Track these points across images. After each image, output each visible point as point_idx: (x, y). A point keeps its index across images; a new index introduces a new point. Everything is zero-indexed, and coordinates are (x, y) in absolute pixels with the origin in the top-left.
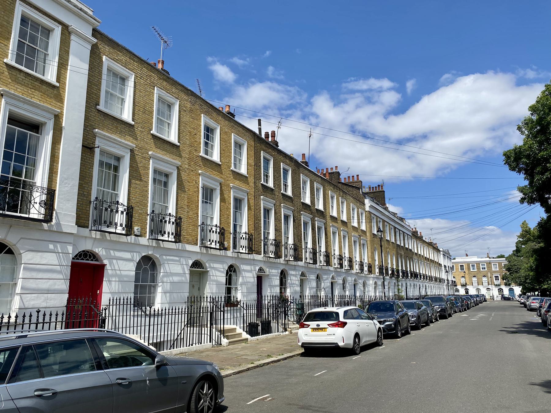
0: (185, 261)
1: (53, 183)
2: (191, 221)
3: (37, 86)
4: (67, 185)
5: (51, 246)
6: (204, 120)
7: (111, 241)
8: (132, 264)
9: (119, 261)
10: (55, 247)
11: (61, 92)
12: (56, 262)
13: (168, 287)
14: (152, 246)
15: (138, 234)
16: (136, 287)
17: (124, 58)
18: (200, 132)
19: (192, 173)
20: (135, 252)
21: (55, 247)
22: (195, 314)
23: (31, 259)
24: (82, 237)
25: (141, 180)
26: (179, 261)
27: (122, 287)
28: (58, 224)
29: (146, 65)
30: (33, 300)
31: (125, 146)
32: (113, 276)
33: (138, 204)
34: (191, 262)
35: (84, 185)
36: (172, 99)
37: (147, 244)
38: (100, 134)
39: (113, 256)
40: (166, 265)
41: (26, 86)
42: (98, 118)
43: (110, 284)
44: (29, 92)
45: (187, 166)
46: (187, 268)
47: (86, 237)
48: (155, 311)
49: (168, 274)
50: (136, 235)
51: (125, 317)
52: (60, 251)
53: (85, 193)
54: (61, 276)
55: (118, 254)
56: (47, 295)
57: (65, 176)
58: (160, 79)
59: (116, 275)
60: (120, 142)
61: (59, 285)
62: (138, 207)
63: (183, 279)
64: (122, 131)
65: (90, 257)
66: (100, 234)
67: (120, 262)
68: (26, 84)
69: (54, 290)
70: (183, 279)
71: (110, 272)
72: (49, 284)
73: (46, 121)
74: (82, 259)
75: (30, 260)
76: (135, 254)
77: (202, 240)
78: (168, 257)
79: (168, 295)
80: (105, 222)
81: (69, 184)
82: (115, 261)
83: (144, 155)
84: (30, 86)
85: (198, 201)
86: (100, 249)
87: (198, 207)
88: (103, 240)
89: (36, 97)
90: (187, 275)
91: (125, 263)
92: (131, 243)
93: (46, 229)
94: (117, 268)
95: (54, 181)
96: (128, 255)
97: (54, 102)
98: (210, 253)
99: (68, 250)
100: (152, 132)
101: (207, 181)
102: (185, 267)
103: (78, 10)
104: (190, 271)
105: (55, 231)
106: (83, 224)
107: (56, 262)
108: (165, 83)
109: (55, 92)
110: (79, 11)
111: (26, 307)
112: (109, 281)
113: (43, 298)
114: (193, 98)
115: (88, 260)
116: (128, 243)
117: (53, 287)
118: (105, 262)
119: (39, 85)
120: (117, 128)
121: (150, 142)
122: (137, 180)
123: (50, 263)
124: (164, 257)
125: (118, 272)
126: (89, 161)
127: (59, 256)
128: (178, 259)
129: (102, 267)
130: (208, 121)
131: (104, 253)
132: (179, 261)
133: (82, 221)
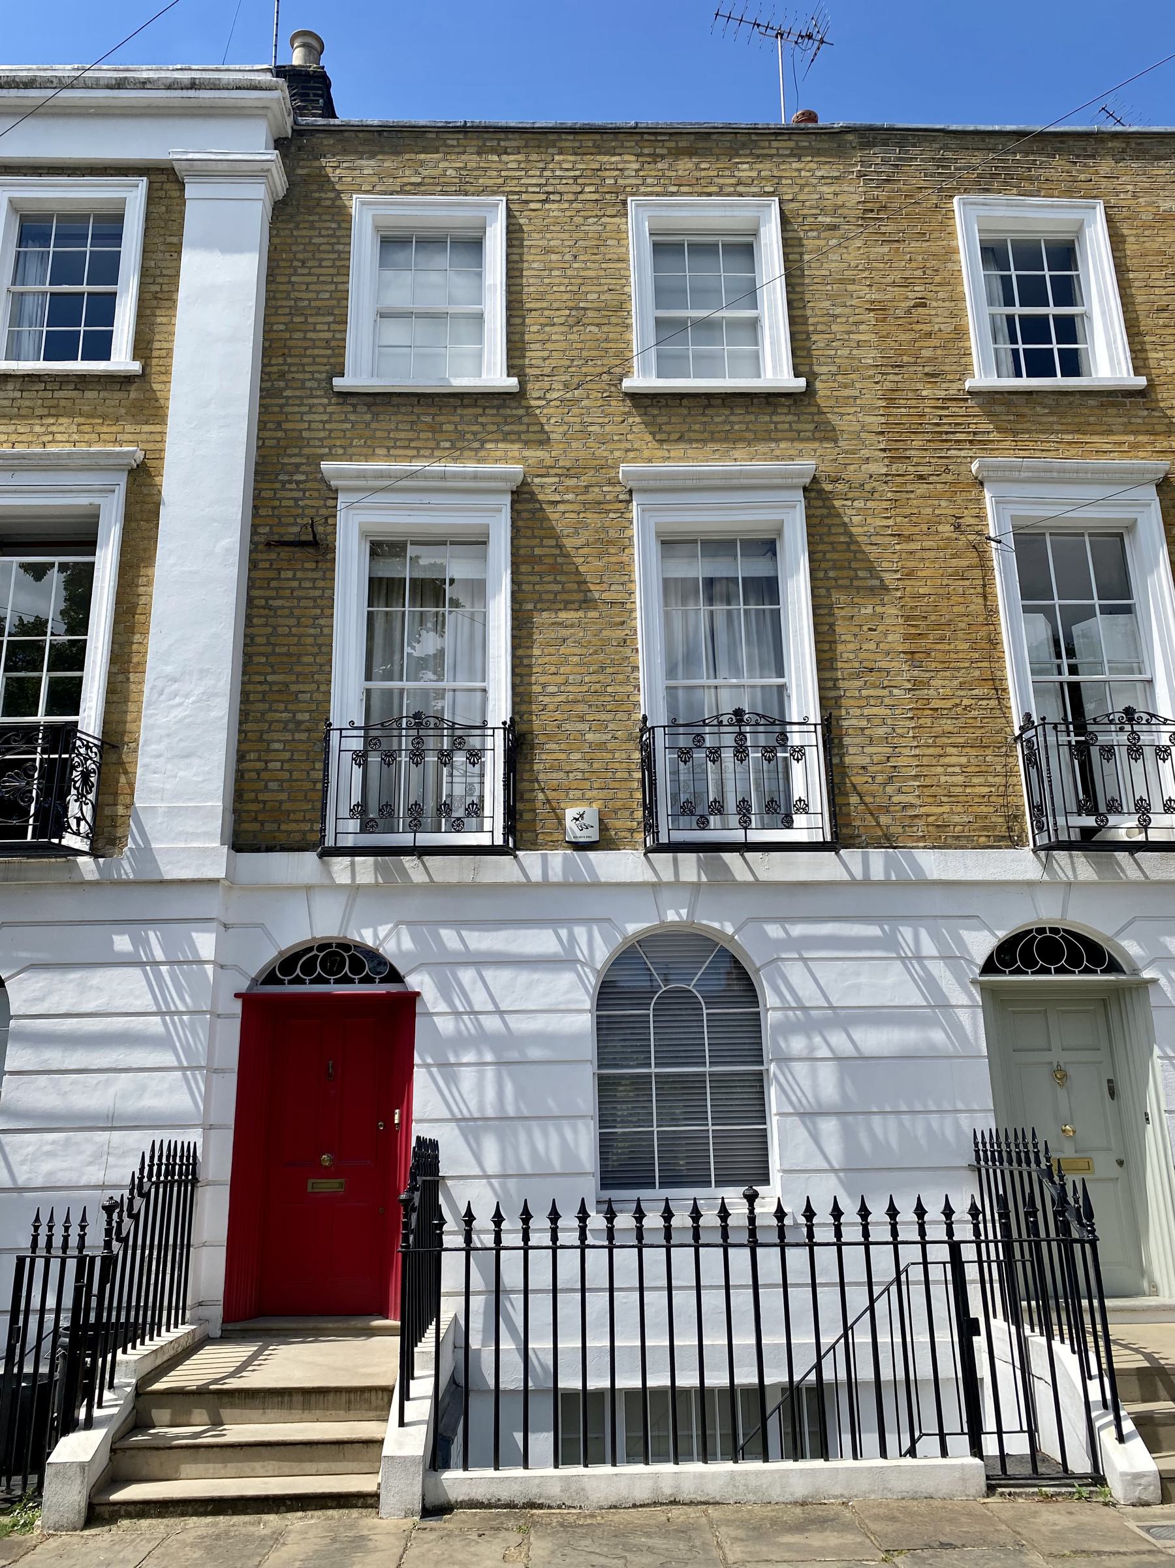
0: (935, 936)
1: (132, 707)
2: (948, 725)
3: (62, 403)
4: (178, 700)
5: (122, 943)
6: (968, 221)
7: (433, 888)
8: (567, 978)
9: (489, 974)
10: (139, 941)
11: (155, 386)
12: (146, 1002)
13: (827, 1084)
14: (677, 884)
15: (584, 836)
16: (605, 1085)
17: (447, 165)
18: (953, 281)
19: (922, 489)
20: (586, 921)
21: (139, 941)
22: (541, 1277)
23: (42, 999)
24: (292, 889)
25: (587, 603)
26: (890, 942)
27: (519, 1093)
28: (146, 853)
29: (568, 142)
30: (51, 1154)
31: (475, 487)
32: (460, 1042)
33: (582, 708)
34: (982, 944)
35: (294, 688)
36: (737, 212)
37: (650, 877)
38: (341, 475)
39: (456, 953)
40: (796, 973)
41: (25, 417)
42: (346, 421)
43: (452, 1079)
44: (37, 429)
45: (879, 468)
46: (959, 977)
47: (309, 888)
48: (780, 1214)
49: (812, 1021)
50: (578, 846)
51: (55, 1264)
52: (159, 955)
53: (299, 717)
54: (169, 1059)
55: (481, 941)
56: (106, 1135)
57: (169, 669)
58: (655, 157)
59: (482, 1039)
60: (443, 476)
61: (158, 1094)
62: (582, 719)
63: (938, 1036)
64: (462, 435)
65: (357, 966)
66: (376, 866)
67: (498, 978)
68: (23, 412)
69: (137, 1116)
70: (938, 1036)
71: (446, 1025)
72: (112, 1091)
73: (96, 501)
74: (320, 980)
75: (36, 1000)
76: (580, 932)
77: (1038, 810)
78: (797, 930)
79: (829, 1127)
80: (416, 811)
81: (187, 696)
82: (467, 976)
83: (595, 494)
84: (39, 412)
85: (992, 612)
86: (383, 930)
87: (994, 642)
88: (391, 890)
89: (59, 437)
90: (964, 1016)
91: (524, 977)
92: (546, 884)
93: (89, 877)
94: (480, 1000)
95: (133, 697)
96: (542, 942)
97: (129, 428)
98: (1133, 874)
99: (194, 949)
100: (627, 384)
101: (1023, 501)
102: (939, 970)
103: (185, 93)
104: (985, 989)
105: (128, 883)
106: (297, 837)
107: (146, 1002)
108: (685, 165)
109: (133, 395)
110: (192, 93)
111: (21, 1181)
112: (444, 1065)
113: (89, 1149)
114: (877, 154)
115: (346, 980)
116: (529, 885)
117: (132, 1106)
118: (415, 981)
119: (74, 394)
120: (435, 429)
121: (624, 428)
122: (567, 605)
123: (119, 1005)
124: (774, 931)
125: (492, 1023)
126: (312, 593)
127: (159, 977)
128: (873, 931)
129: (402, 1009)
130: (984, 211)
131: (407, 944)
132: (890, 942)
133: (293, 826)
